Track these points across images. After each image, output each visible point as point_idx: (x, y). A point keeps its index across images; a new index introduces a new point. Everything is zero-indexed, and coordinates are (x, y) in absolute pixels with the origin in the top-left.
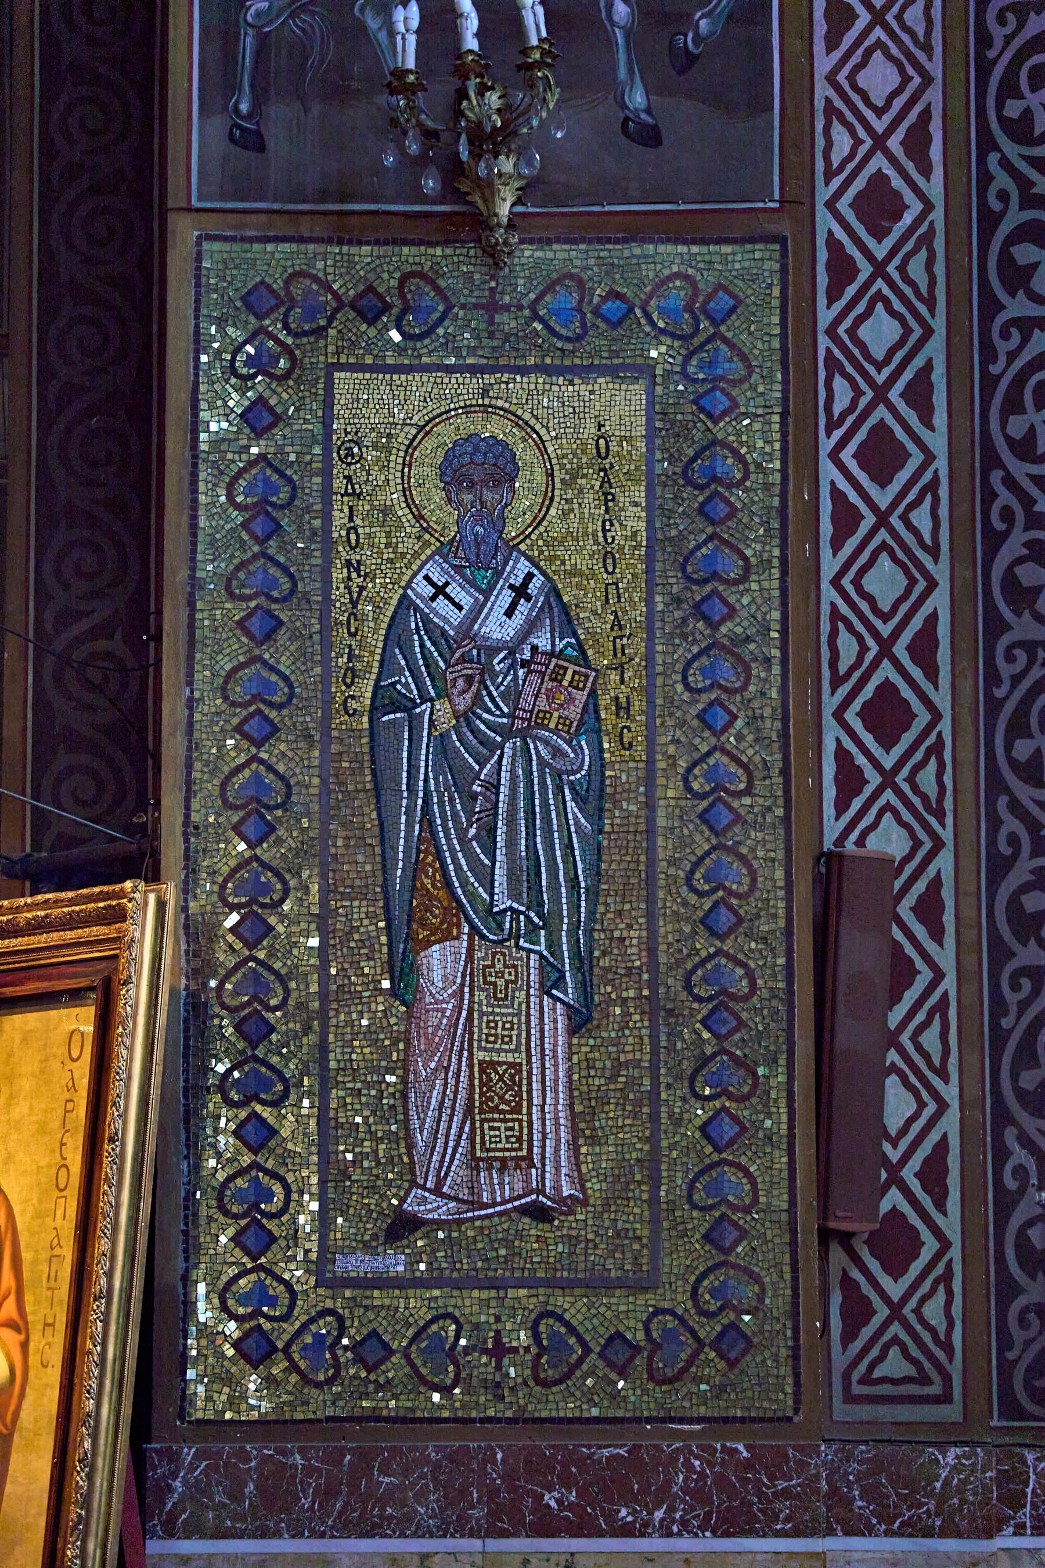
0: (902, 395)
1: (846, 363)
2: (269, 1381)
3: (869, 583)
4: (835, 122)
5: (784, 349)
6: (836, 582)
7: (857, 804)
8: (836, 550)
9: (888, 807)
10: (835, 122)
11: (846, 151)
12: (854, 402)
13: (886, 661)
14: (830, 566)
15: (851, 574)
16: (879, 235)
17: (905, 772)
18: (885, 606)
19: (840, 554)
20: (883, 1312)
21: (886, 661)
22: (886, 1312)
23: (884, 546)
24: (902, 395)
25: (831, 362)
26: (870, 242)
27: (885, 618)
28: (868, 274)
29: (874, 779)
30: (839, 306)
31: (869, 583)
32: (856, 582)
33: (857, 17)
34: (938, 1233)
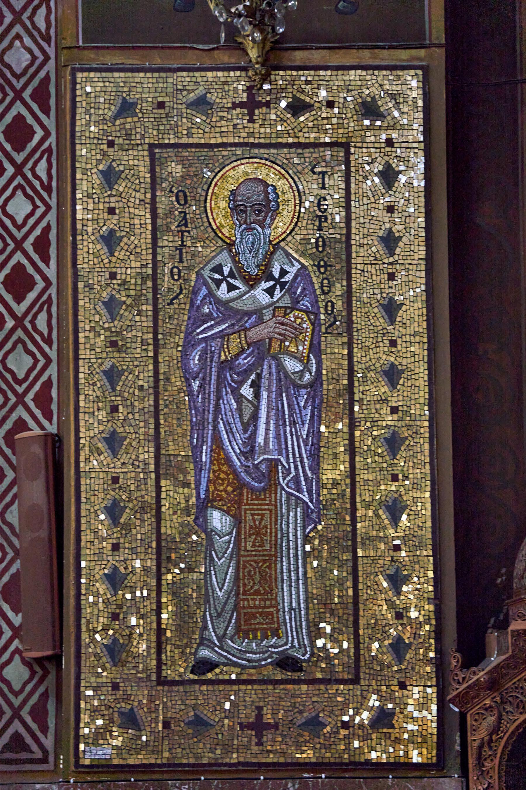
0: (4, 713)
1: (39, 188)
2: (420, 753)
3: (29, 361)
4: (43, 31)
5: (74, 90)
6: (49, 361)
7: (38, 232)
8: (49, 380)
9: (16, 694)
10: (43, 31)
11: (39, 317)
12: (35, 316)
13: (18, 102)
14: (53, 371)
15: (37, 63)
16: (19, 266)
17: (30, 164)
18: (17, 687)
19: (49, 734)
20: (29, 399)
21: (18, 102)
22: (26, 399)
23: (19, 186)
24: (4, 713)
25: (48, 189)
26: (22, 731)
27: (16, 694)
28: (23, 710)
29: (25, 713)
30: (44, 378)
31: (29, 361)
32: (36, 361)
33: (29, 713)
34: (45, 278)
